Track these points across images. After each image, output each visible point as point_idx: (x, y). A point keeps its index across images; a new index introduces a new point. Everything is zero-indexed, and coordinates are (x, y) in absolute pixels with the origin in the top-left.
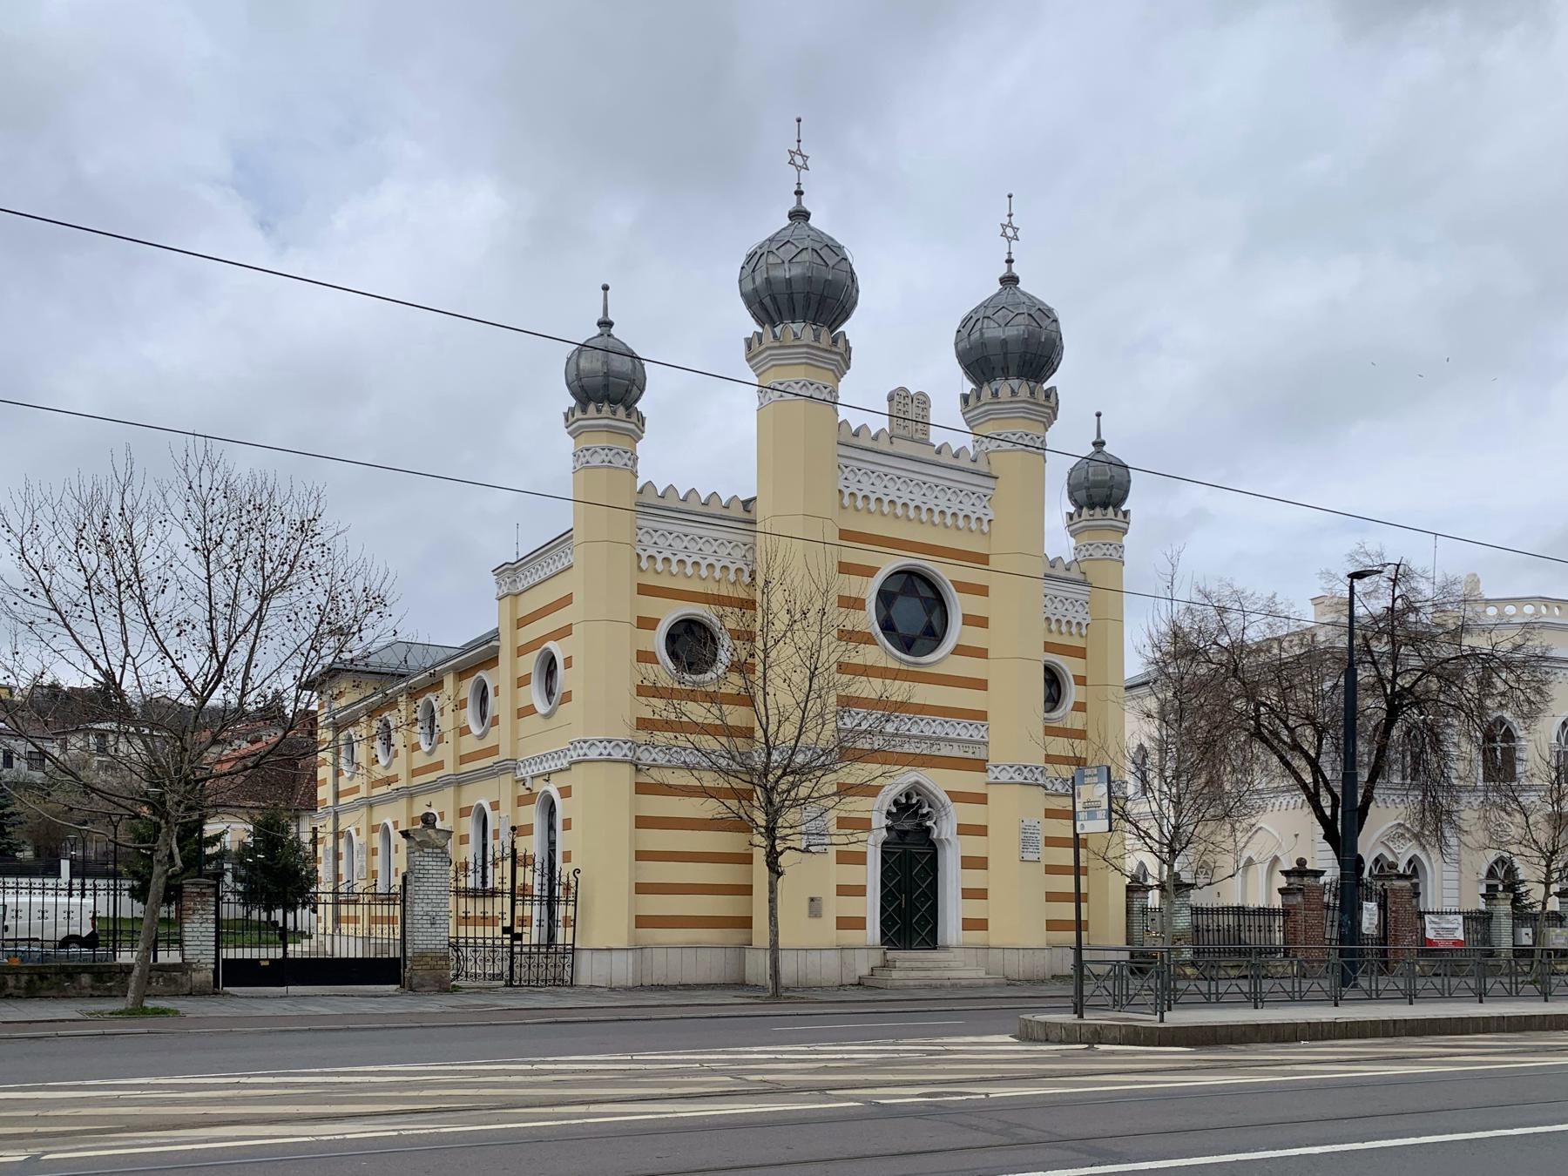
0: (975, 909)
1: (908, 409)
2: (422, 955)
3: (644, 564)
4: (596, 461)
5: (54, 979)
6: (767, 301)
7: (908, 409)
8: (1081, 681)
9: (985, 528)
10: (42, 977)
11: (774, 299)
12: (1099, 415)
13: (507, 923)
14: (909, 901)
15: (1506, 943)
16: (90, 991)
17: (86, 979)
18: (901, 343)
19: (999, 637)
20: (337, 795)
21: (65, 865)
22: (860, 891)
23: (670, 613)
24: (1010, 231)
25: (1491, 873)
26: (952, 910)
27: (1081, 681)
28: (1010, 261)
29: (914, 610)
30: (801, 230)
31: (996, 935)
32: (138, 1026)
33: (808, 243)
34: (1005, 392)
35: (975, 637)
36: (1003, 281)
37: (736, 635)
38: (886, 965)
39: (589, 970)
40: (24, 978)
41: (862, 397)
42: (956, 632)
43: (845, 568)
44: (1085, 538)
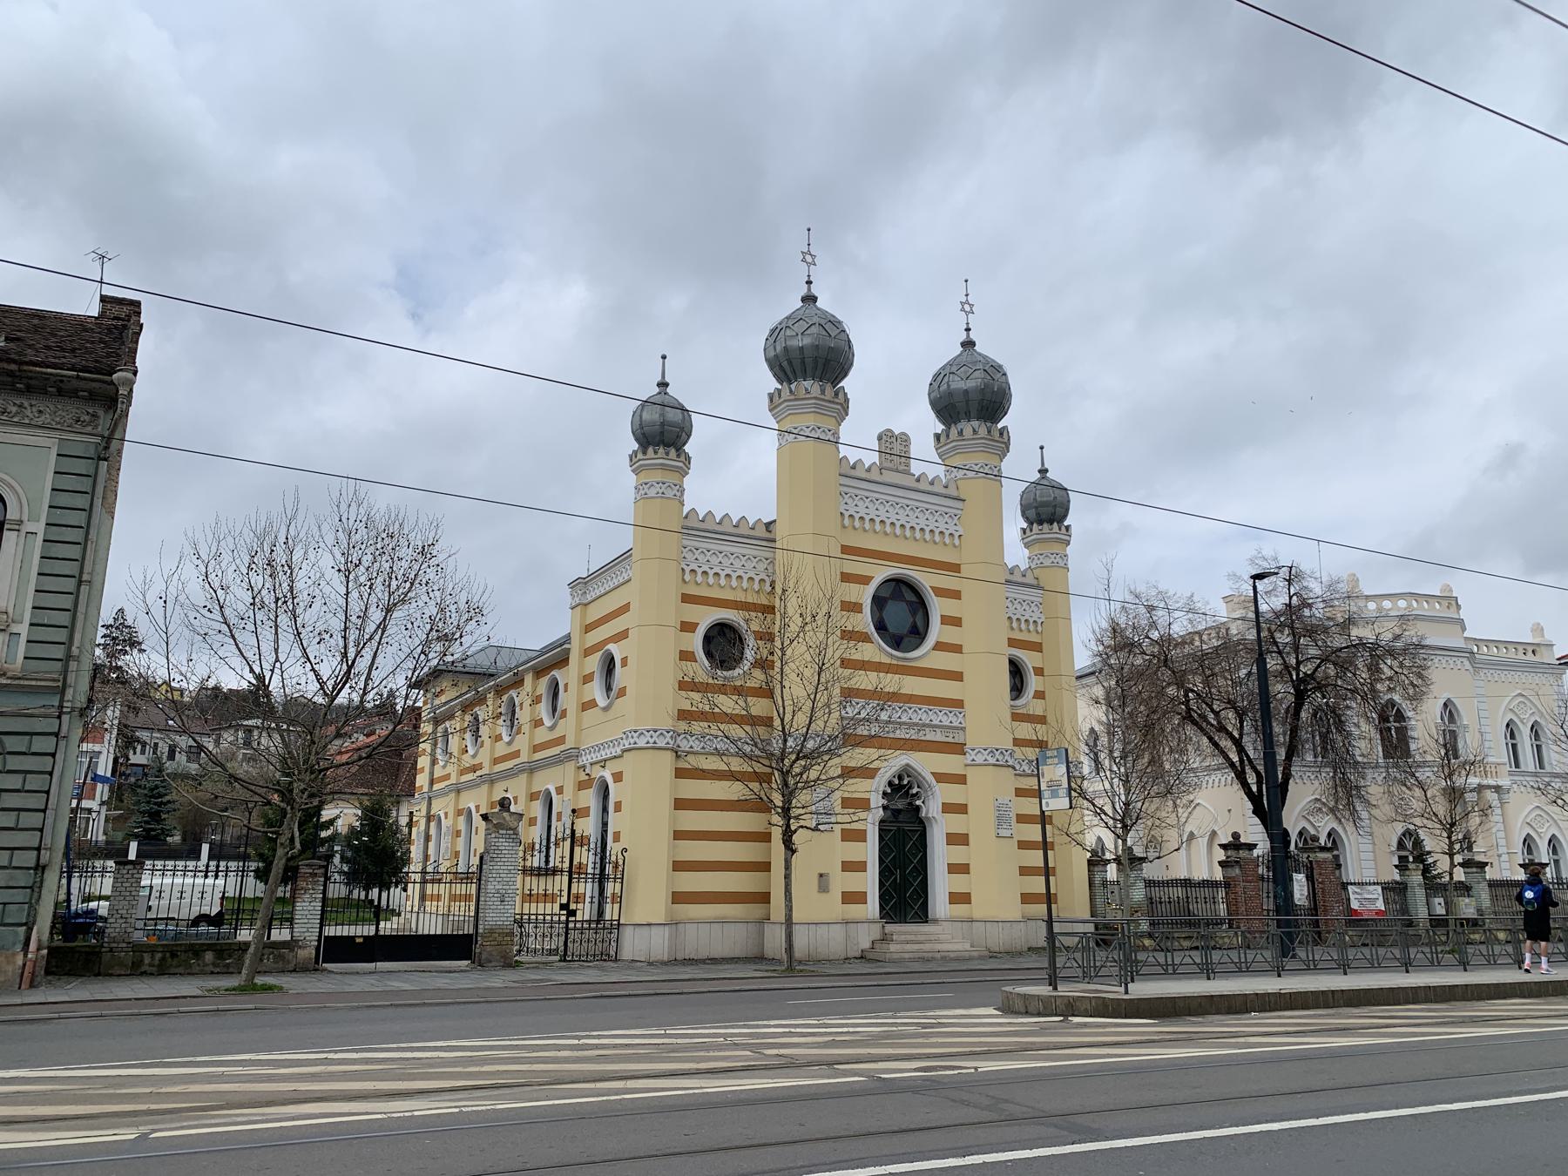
0: (959, 883)
1: (893, 446)
2: (492, 931)
3: (1015, 625)
4: (652, 492)
5: (183, 957)
6: (785, 364)
7: (893, 446)
8: (1039, 672)
9: (957, 542)
10: (174, 955)
11: (790, 363)
12: (664, 357)
13: (564, 901)
14: (903, 877)
15: (1422, 913)
16: (211, 968)
17: (209, 956)
18: (888, 395)
19: (970, 631)
20: (432, 782)
21: (205, 848)
22: (860, 867)
23: (707, 617)
24: (967, 307)
25: (1401, 845)
26: (941, 884)
27: (1039, 672)
28: (968, 330)
29: (902, 612)
30: (811, 311)
31: (977, 909)
32: (247, 1002)
33: (816, 320)
34: (968, 432)
35: (951, 635)
36: (963, 344)
37: (759, 636)
38: (885, 938)
39: (632, 945)
40: (159, 955)
41: (858, 438)
42: (936, 632)
43: (846, 578)
44: (1037, 549)
